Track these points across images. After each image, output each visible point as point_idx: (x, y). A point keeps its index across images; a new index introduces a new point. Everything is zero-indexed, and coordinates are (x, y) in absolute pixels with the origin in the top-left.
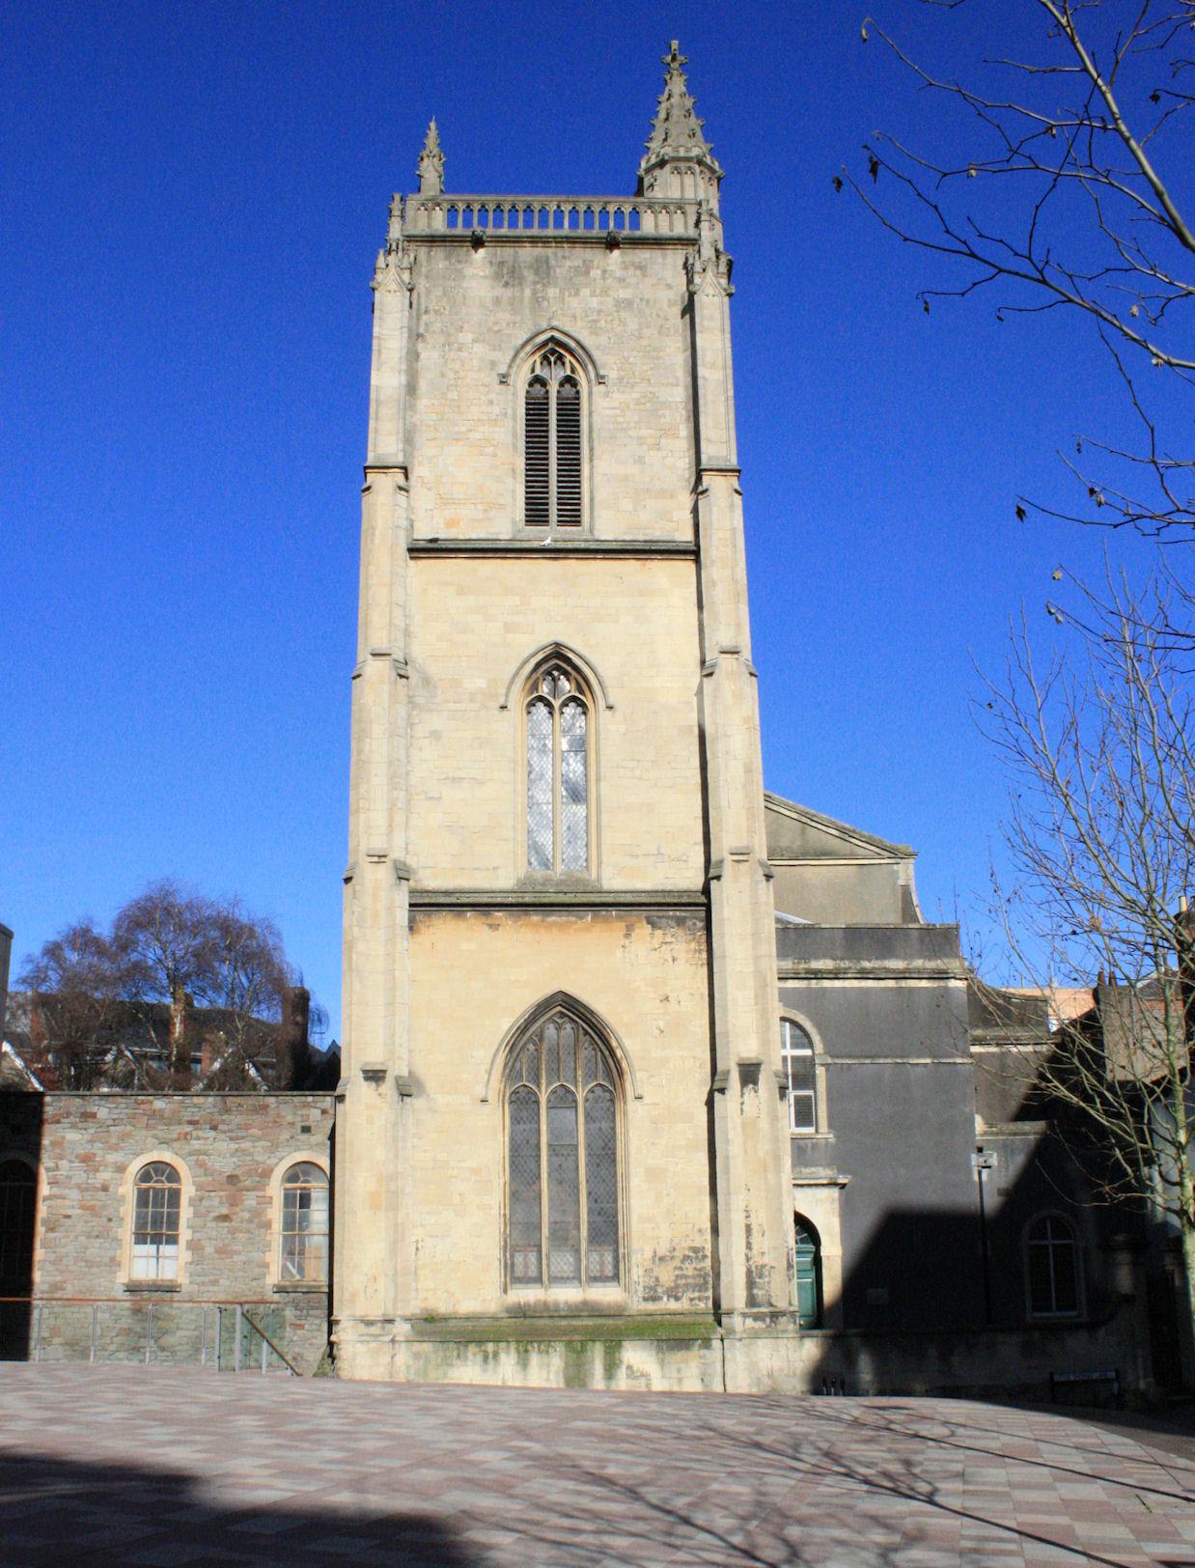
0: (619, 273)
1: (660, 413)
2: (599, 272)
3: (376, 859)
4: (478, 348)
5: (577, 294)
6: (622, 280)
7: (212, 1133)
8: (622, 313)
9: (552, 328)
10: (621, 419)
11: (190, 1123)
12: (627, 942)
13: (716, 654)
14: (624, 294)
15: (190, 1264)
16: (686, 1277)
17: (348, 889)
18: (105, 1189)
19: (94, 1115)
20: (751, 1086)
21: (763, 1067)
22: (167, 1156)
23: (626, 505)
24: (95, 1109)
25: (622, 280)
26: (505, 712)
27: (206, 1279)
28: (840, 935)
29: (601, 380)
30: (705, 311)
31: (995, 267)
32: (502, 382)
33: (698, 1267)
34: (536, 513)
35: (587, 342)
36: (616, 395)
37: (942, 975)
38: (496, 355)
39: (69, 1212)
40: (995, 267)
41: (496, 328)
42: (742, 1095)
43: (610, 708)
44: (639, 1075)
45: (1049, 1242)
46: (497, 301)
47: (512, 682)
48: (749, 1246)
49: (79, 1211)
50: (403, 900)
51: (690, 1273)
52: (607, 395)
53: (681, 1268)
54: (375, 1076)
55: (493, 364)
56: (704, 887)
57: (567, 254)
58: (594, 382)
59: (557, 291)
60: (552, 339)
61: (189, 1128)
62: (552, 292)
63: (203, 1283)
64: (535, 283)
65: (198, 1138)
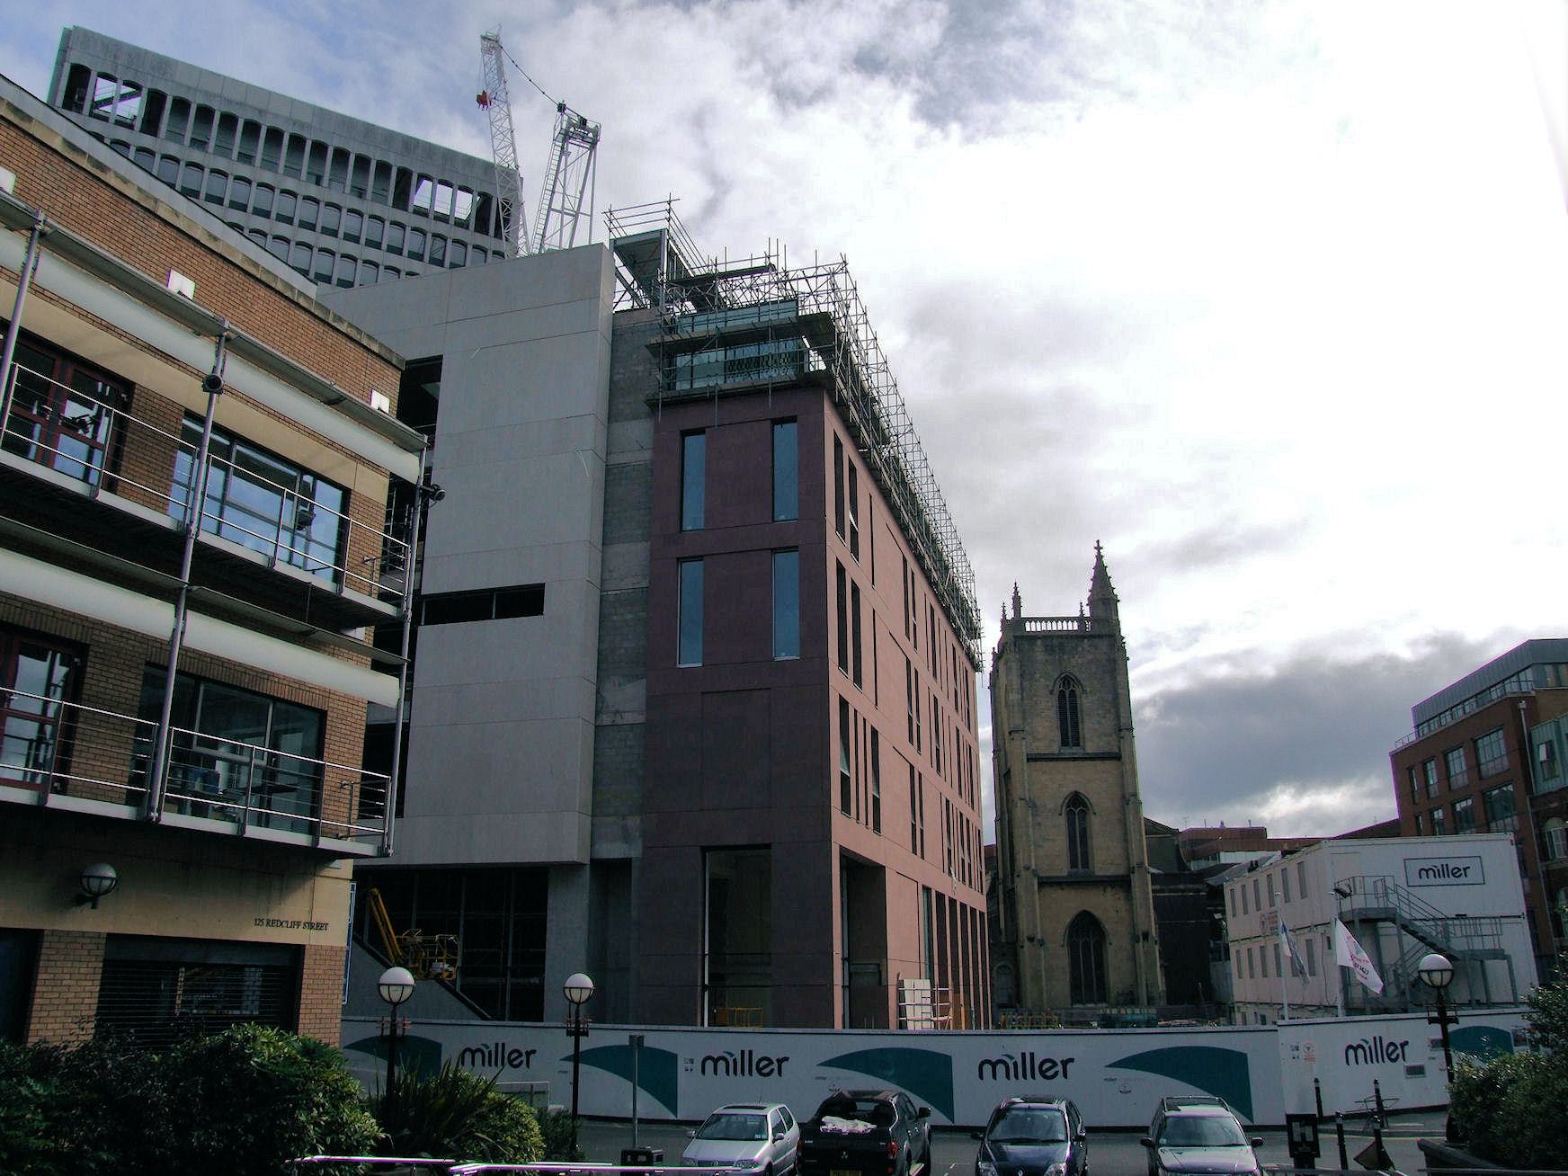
4: (1042, 680)
6: (1089, 651)
25: (1089, 651)
28: (322, 174)
31: (592, 212)
34: (1064, 743)
35: (1079, 677)
37: (1198, 891)
38: (1048, 683)
40: (592, 212)
46: (1047, 661)
47: (1062, 806)
54: (1031, 939)
55: (1048, 686)
62: (1065, 657)
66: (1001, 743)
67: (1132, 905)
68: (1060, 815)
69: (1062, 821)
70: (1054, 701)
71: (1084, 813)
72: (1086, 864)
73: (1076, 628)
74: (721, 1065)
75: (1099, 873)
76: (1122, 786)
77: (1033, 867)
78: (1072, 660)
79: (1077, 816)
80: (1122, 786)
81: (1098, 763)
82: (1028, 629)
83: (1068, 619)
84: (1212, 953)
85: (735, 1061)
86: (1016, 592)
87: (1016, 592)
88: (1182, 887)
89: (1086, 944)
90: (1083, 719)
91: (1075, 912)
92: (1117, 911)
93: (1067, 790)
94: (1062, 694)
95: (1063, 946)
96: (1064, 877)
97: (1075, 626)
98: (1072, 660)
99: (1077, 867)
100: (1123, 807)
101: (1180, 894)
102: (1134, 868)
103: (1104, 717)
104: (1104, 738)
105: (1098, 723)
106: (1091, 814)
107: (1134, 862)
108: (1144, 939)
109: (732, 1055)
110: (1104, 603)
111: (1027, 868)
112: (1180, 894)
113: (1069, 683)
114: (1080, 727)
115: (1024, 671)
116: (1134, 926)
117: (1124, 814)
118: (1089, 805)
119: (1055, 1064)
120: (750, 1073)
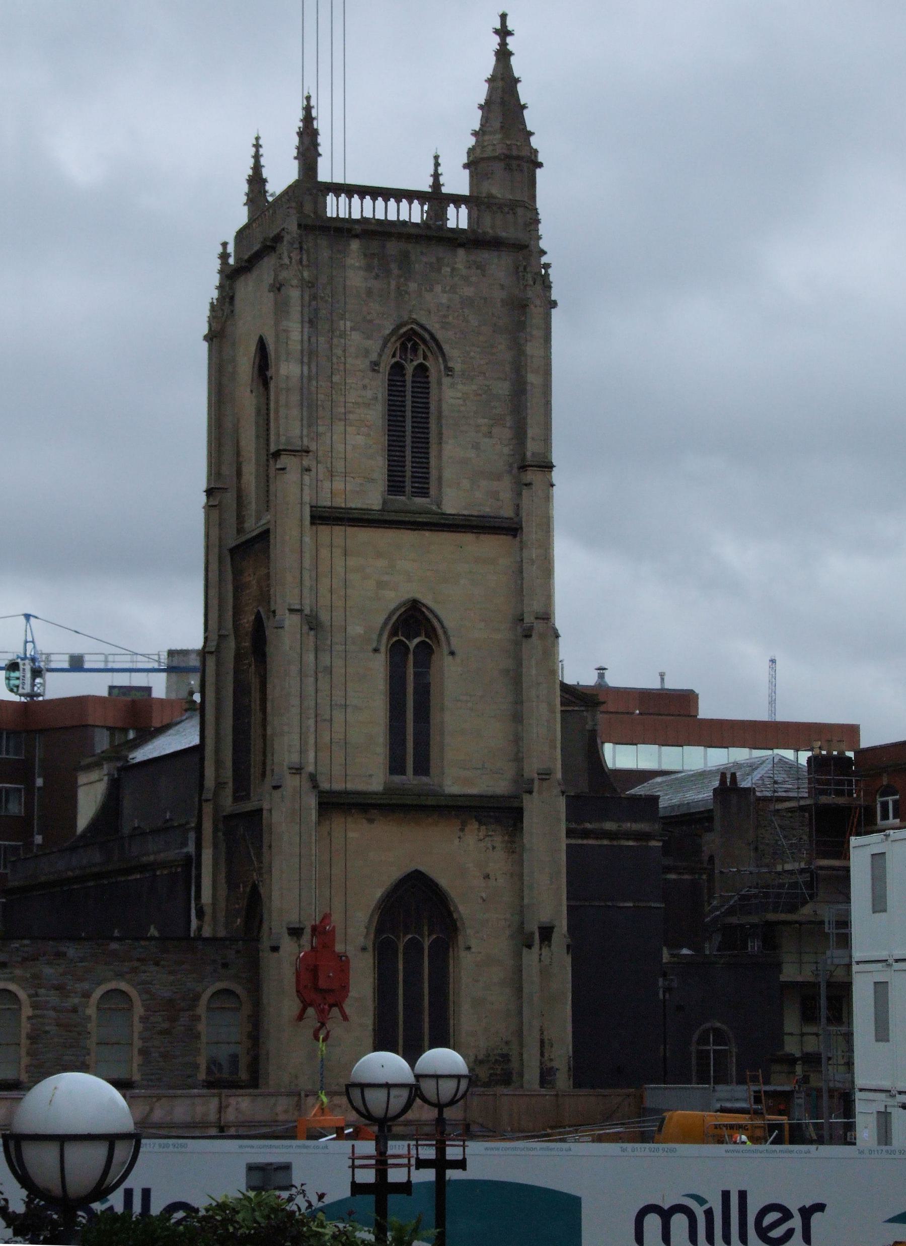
0: (464, 272)
1: (492, 404)
2: (449, 269)
3: (294, 771)
5: (431, 290)
7: (156, 968)
8: (466, 310)
9: (412, 323)
10: (463, 408)
11: (138, 960)
12: (461, 834)
13: (532, 619)
14: (468, 291)
15: (142, 1065)
16: (496, 1074)
17: (277, 794)
18: (75, 1010)
19: (65, 954)
20: (546, 943)
21: (555, 930)
22: (123, 986)
23: (466, 484)
24: (63, 949)
25: (466, 279)
26: (377, 655)
27: (153, 1077)
29: (449, 370)
30: (534, 321)
32: (374, 370)
33: (505, 1067)
34: (395, 485)
35: (439, 335)
36: (460, 387)
38: (369, 343)
39: (47, 1028)
41: (368, 318)
42: (541, 949)
43: (452, 653)
44: (469, 931)
45: (711, 1047)
46: (369, 292)
47: (380, 635)
48: (542, 1055)
49: (54, 1028)
50: (312, 802)
51: (499, 1072)
52: (453, 385)
53: (493, 1068)
55: (367, 352)
56: (165, 672)
57: (424, 251)
58: (443, 373)
59: (416, 285)
60: (412, 329)
61: (136, 964)
62: (413, 286)
63: (151, 1080)
64: (400, 277)
65: (145, 972)
66: (228, 470)
67: (521, 863)
68: (376, 650)
69: (379, 666)
70: (378, 386)
71: (426, 652)
72: (423, 767)
73: (416, 218)
74: (679, 1222)
75: (452, 787)
76: (519, 592)
77: (311, 768)
78: (428, 296)
79: (411, 657)
80: (519, 592)
81: (468, 538)
82: (451, 224)
83: (399, 195)
84: (665, 975)
85: (709, 1213)
86: (308, 119)
87: (308, 119)
88: (610, 826)
89: (414, 947)
90: (440, 434)
91: (395, 874)
92: (487, 877)
93: (407, 591)
94: (397, 369)
95: (364, 949)
96: (376, 794)
97: (415, 213)
98: (428, 296)
99: (403, 772)
100: (517, 644)
101: (606, 842)
102: (532, 781)
103: (489, 435)
104: (484, 483)
105: (476, 446)
106: (445, 650)
107: (532, 767)
108: (542, 940)
109: (701, 1201)
110: (508, 168)
111: (297, 770)
112: (606, 842)
113: (415, 349)
114: (433, 452)
115: (316, 310)
116: (521, 910)
117: (519, 664)
118: (440, 632)
119: (787, 1215)
120: (743, 1238)
